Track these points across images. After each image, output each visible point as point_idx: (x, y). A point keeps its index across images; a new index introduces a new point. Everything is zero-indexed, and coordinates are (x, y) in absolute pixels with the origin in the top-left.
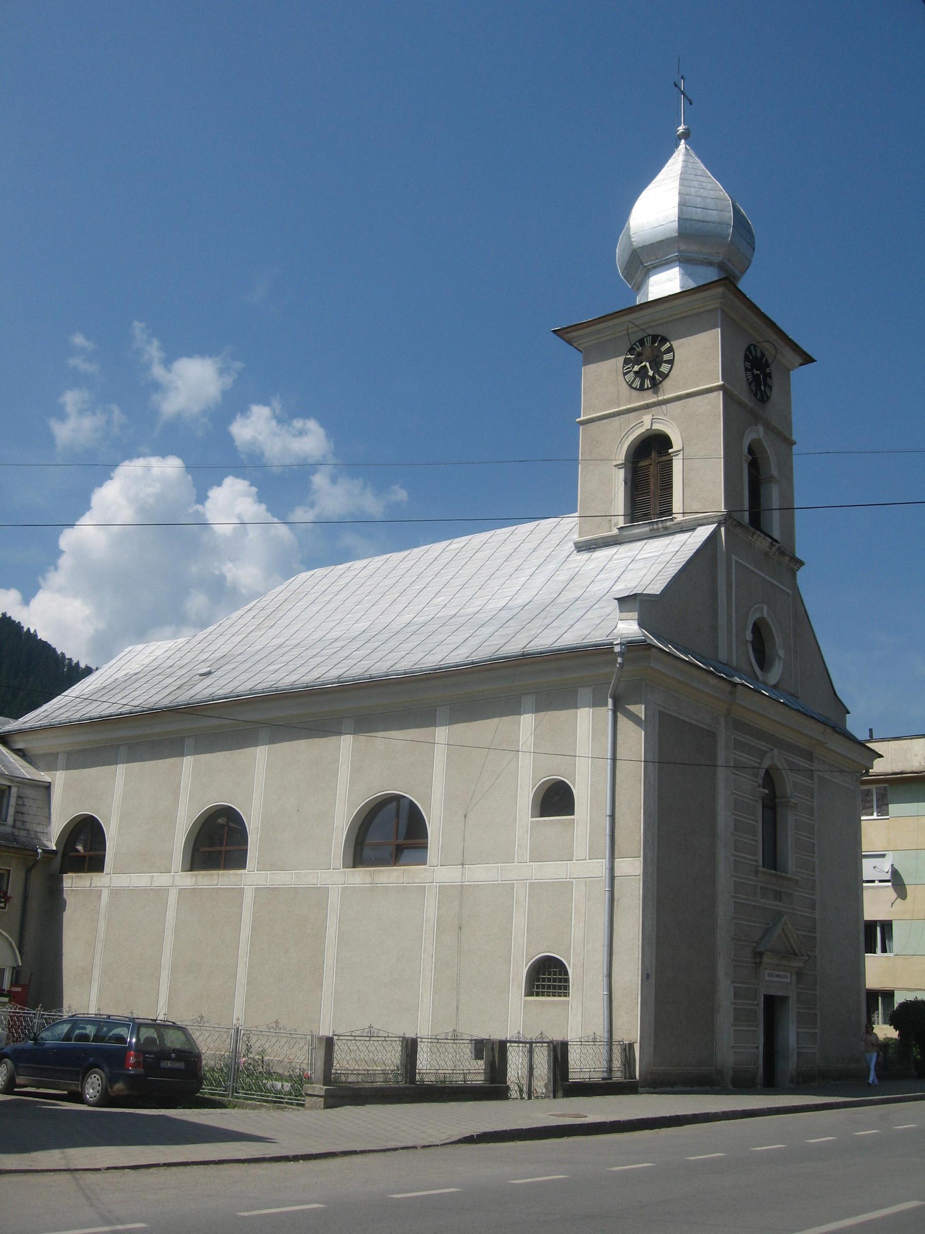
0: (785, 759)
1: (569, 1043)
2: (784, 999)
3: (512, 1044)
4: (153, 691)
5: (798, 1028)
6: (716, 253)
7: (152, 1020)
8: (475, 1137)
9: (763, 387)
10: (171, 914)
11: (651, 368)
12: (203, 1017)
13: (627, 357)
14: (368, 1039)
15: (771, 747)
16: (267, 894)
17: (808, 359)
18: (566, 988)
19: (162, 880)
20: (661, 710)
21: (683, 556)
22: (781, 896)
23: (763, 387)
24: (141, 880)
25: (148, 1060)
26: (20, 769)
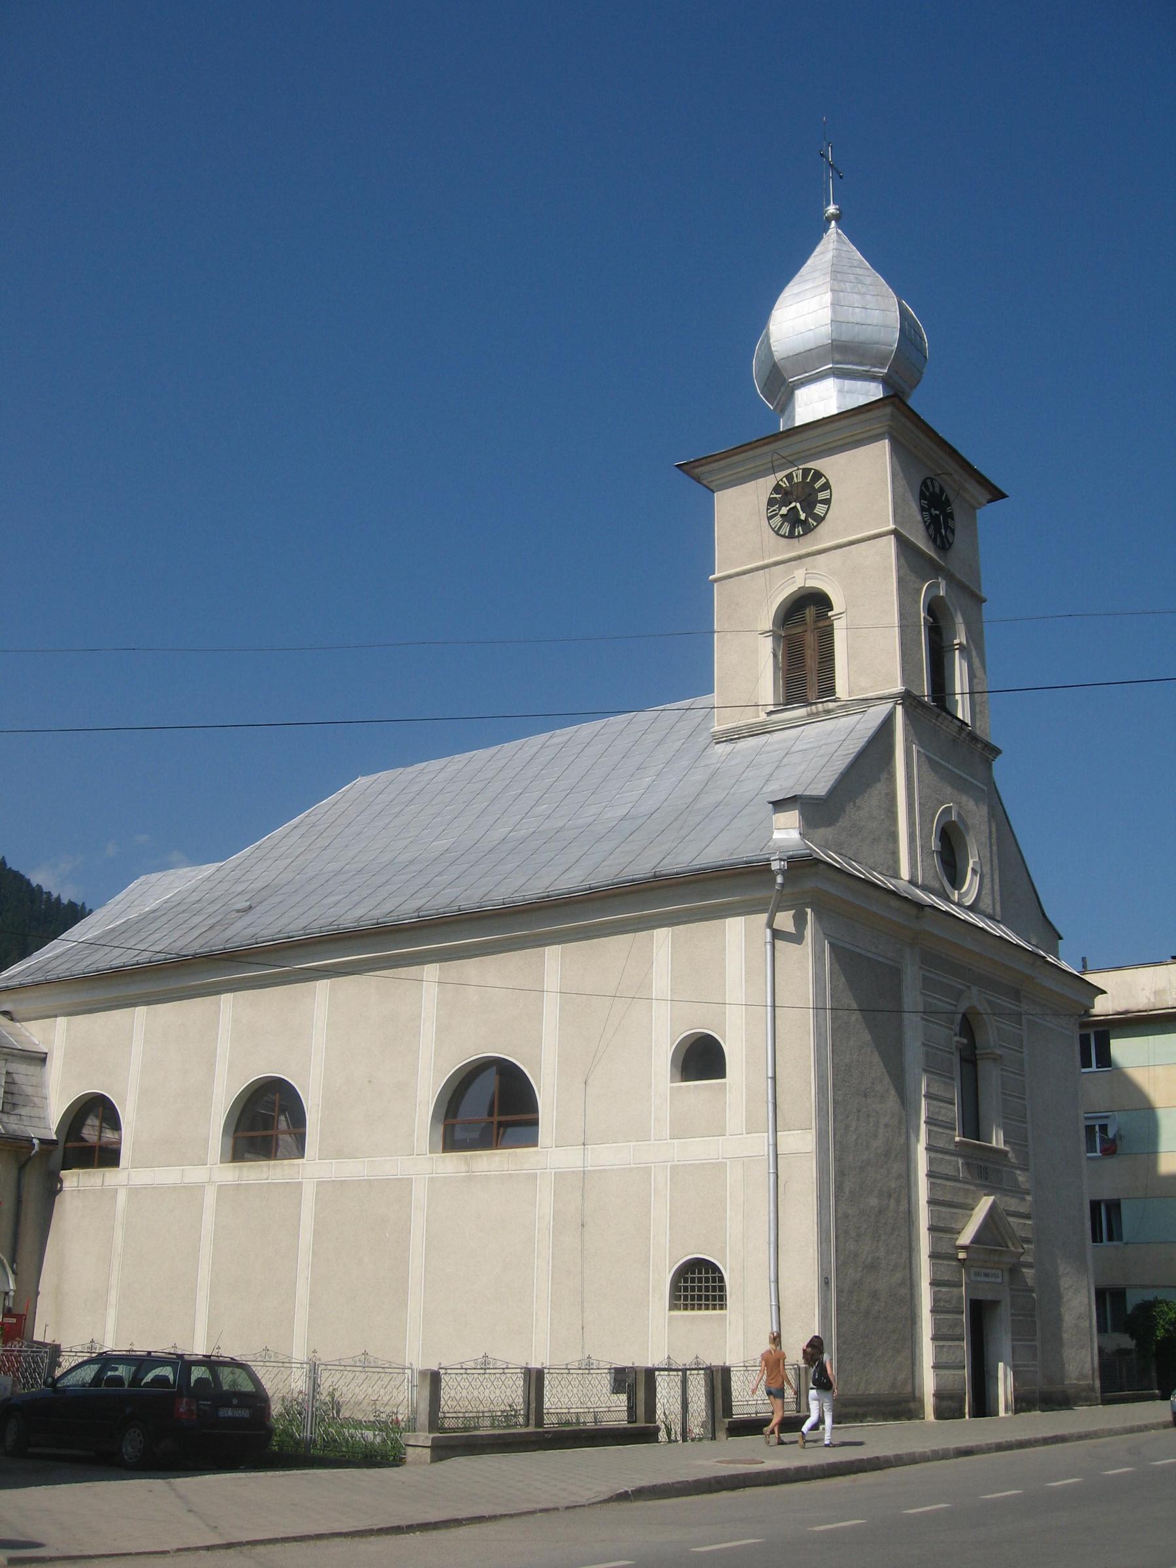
0: (986, 999)
1: (732, 1369)
2: (995, 1303)
3: (662, 1373)
4: (176, 935)
5: (1013, 1340)
7: (127, 1351)
8: (630, 1493)
9: (943, 531)
10: (208, 1217)
11: (802, 510)
12: (268, 1350)
13: (772, 496)
14: (482, 1371)
16: (331, 1190)
17: (997, 495)
18: (722, 1298)
19: (195, 1175)
21: (852, 746)
22: (986, 1173)
23: (943, 531)
24: (168, 1176)
25: (201, 1406)
26: (7, 1037)
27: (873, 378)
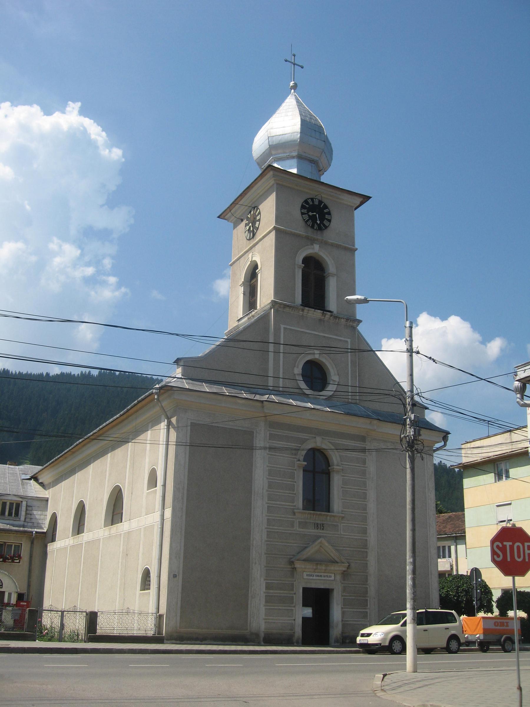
0: (328, 441)
6: (293, 151)
15: (315, 436)
20: (193, 422)
27: (293, 157)
